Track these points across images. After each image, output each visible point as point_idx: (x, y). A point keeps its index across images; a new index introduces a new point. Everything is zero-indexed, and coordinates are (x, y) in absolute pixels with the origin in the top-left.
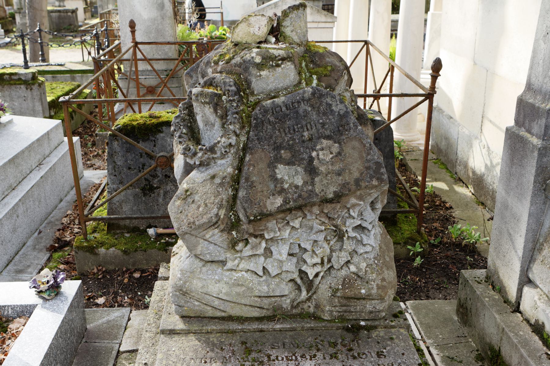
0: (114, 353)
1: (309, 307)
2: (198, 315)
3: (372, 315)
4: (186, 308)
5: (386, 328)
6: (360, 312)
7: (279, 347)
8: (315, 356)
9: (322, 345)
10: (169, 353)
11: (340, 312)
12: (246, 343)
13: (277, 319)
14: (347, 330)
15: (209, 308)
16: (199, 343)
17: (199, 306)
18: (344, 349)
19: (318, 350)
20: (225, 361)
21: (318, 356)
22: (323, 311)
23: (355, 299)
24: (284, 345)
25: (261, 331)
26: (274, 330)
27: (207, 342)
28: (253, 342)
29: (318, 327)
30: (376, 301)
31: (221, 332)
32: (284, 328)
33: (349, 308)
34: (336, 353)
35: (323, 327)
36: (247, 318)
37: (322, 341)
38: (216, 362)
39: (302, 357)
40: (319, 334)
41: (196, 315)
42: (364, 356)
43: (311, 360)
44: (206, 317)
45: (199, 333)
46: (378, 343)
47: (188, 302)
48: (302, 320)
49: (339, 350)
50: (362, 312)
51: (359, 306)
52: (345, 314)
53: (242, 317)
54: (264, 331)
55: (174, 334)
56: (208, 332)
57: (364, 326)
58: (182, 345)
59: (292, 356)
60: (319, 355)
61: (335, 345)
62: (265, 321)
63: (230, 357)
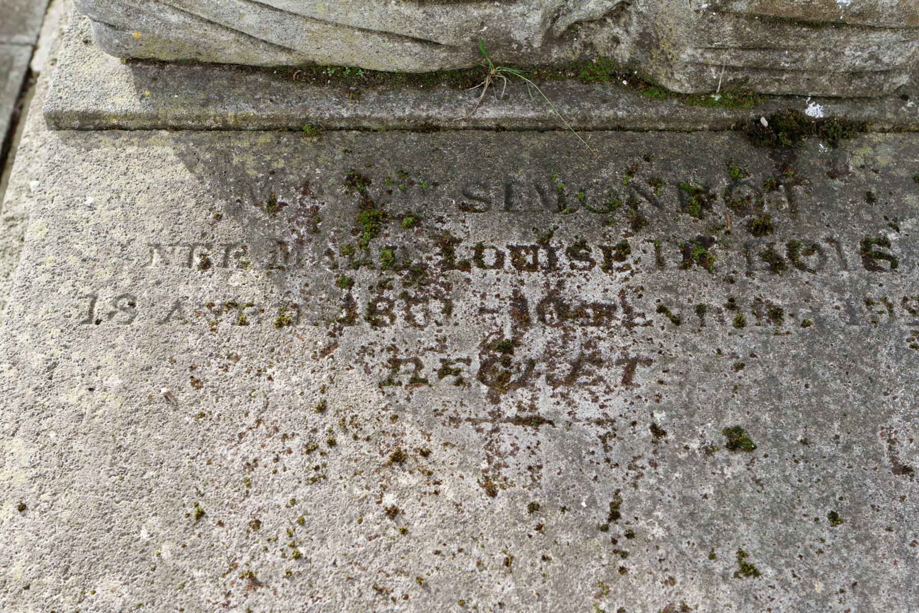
0: (16, 77)
1: (616, 40)
2: (186, 55)
3: (856, 82)
4: (135, 34)
5: (899, 130)
6: (812, 71)
7: (488, 202)
8: (624, 250)
9: (650, 200)
10: (71, 215)
11: (734, 69)
12: (366, 181)
13: (487, 81)
14: (753, 134)
15: (225, 37)
16: (188, 176)
17: (185, 26)
18: (737, 224)
19: (638, 224)
20: (280, 262)
21: (636, 254)
22: (667, 62)
23: (803, 23)
24: (509, 193)
25: (427, 128)
26: (477, 127)
27: (220, 172)
28: (395, 177)
29: (642, 119)
30: (887, 36)
31: (275, 128)
32: (512, 120)
33: (770, 58)
34: (706, 242)
35: (663, 119)
36: (374, 73)
37: (655, 182)
38: (244, 265)
39: (573, 253)
40: (644, 150)
41: (180, 57)
42: (813, 260)
43: (607, 268)
44: (218, 65)
45: (193, 129)
46: (870, 199)
47: (139, 11)
48: (583, 88)
49: (716, 228)
50: (822, 73)
51: (814, 49)
52: (754, 78)
53: (354, 70)
54: (437, 129)
55: (99, 129)
56: (226, 128)
57: (820, 122)
58: (123, 180)
59: (535, 249)
60: (641, 247)
61: (697, 201)
62: (443, 90)
63: (300, 242)
